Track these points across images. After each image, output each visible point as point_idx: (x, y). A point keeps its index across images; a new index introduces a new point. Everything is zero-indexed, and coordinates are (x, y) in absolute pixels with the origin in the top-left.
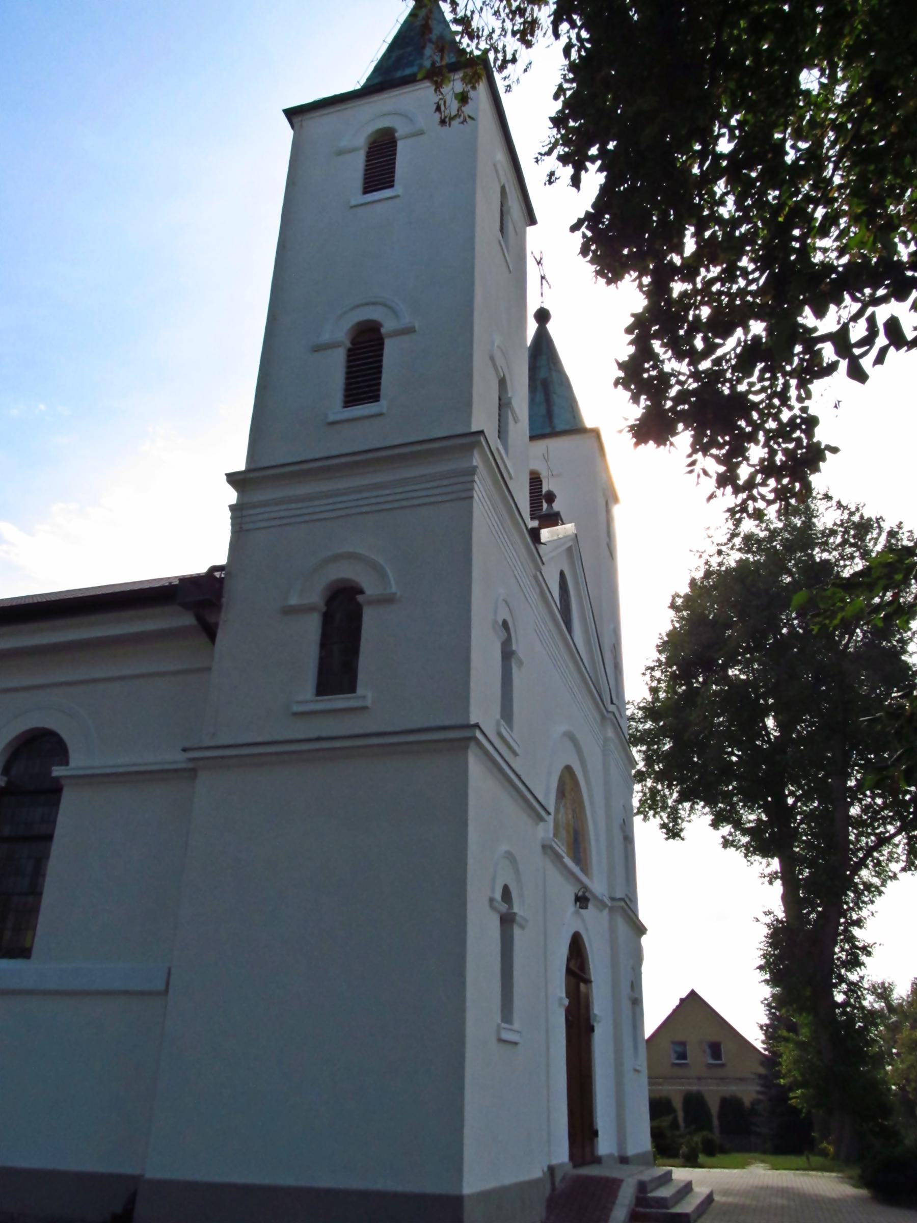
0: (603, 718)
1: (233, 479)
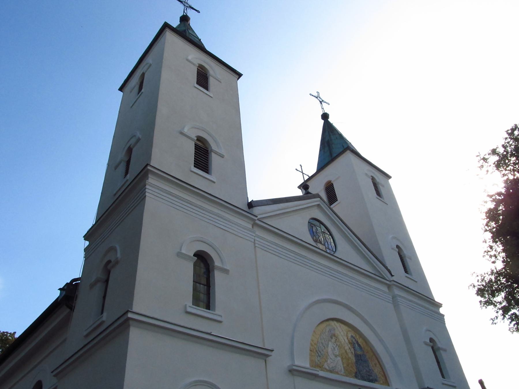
0: (389, 287)
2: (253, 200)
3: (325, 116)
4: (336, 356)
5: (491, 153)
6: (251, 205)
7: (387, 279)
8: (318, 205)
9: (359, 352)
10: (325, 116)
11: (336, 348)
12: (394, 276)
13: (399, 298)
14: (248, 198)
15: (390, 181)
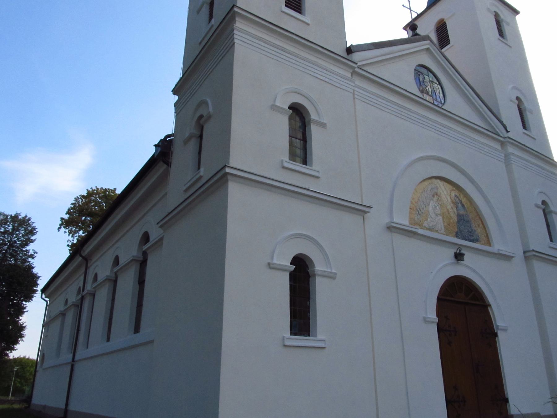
0: (502, 144)
1: (155, 146)
4: (437, 215)
5: (460, 251)
6: (350, 50)
7: (501, 135)
8: (428, 49)
9: (462, 212)
12: (509, 132)
13: (512, 157)
14: (346, 42)
15: (518, 17)
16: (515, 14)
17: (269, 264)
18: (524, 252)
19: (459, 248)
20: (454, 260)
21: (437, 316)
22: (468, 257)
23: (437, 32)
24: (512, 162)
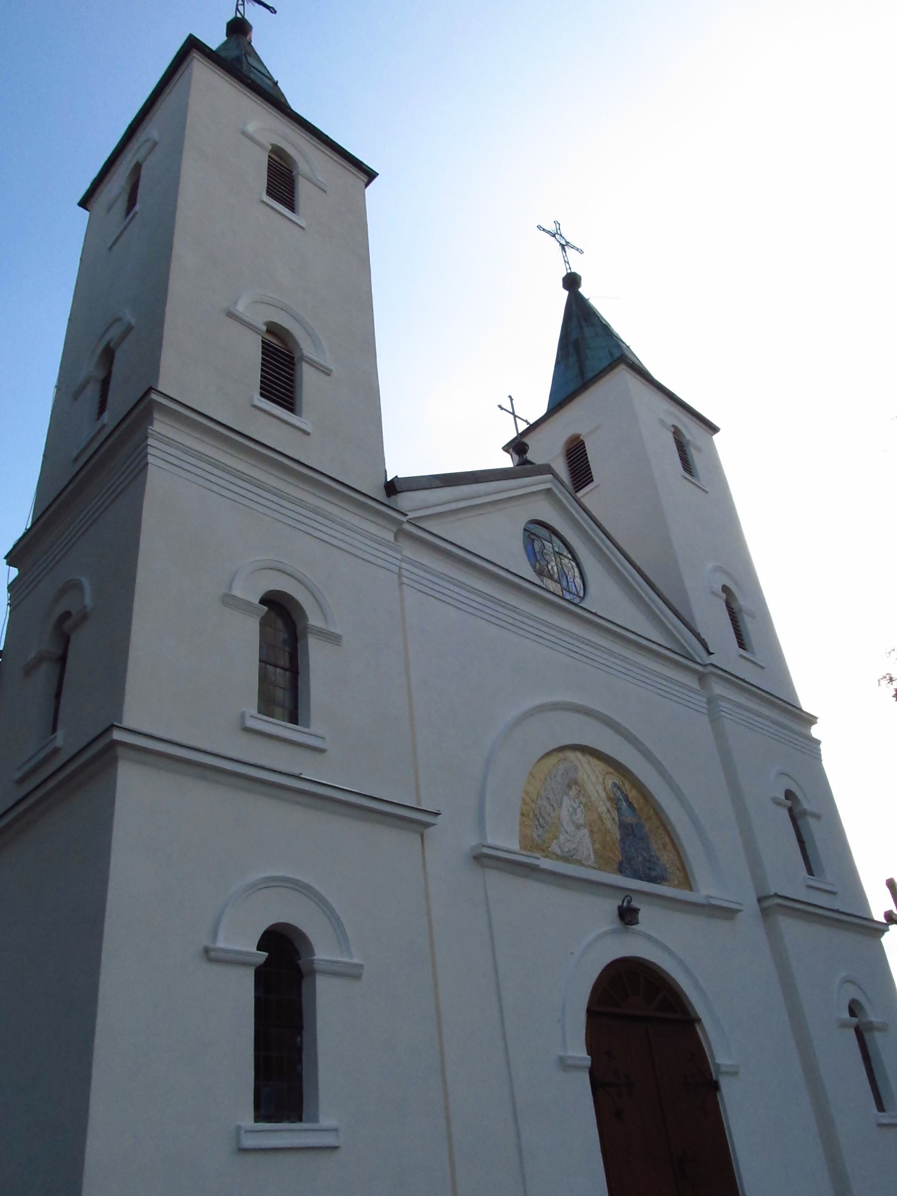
0: (702, 678)
2: (397, 476)
3: (572, 282)
4: (578, 827)
5: (629, 902)
6: (393, 488)
8: (549, 491)
10: (572, 282)
11: (579, 810)
14: (386, 470)
15: (716, 438)
16: (711, 432)
17: (207, 950)
18: (760, 900)
19: (626, 896)
20: (617, 924)
21: (588, 1054)
22: (647, 914)
23: (569, 463)
24: (723, 713)
